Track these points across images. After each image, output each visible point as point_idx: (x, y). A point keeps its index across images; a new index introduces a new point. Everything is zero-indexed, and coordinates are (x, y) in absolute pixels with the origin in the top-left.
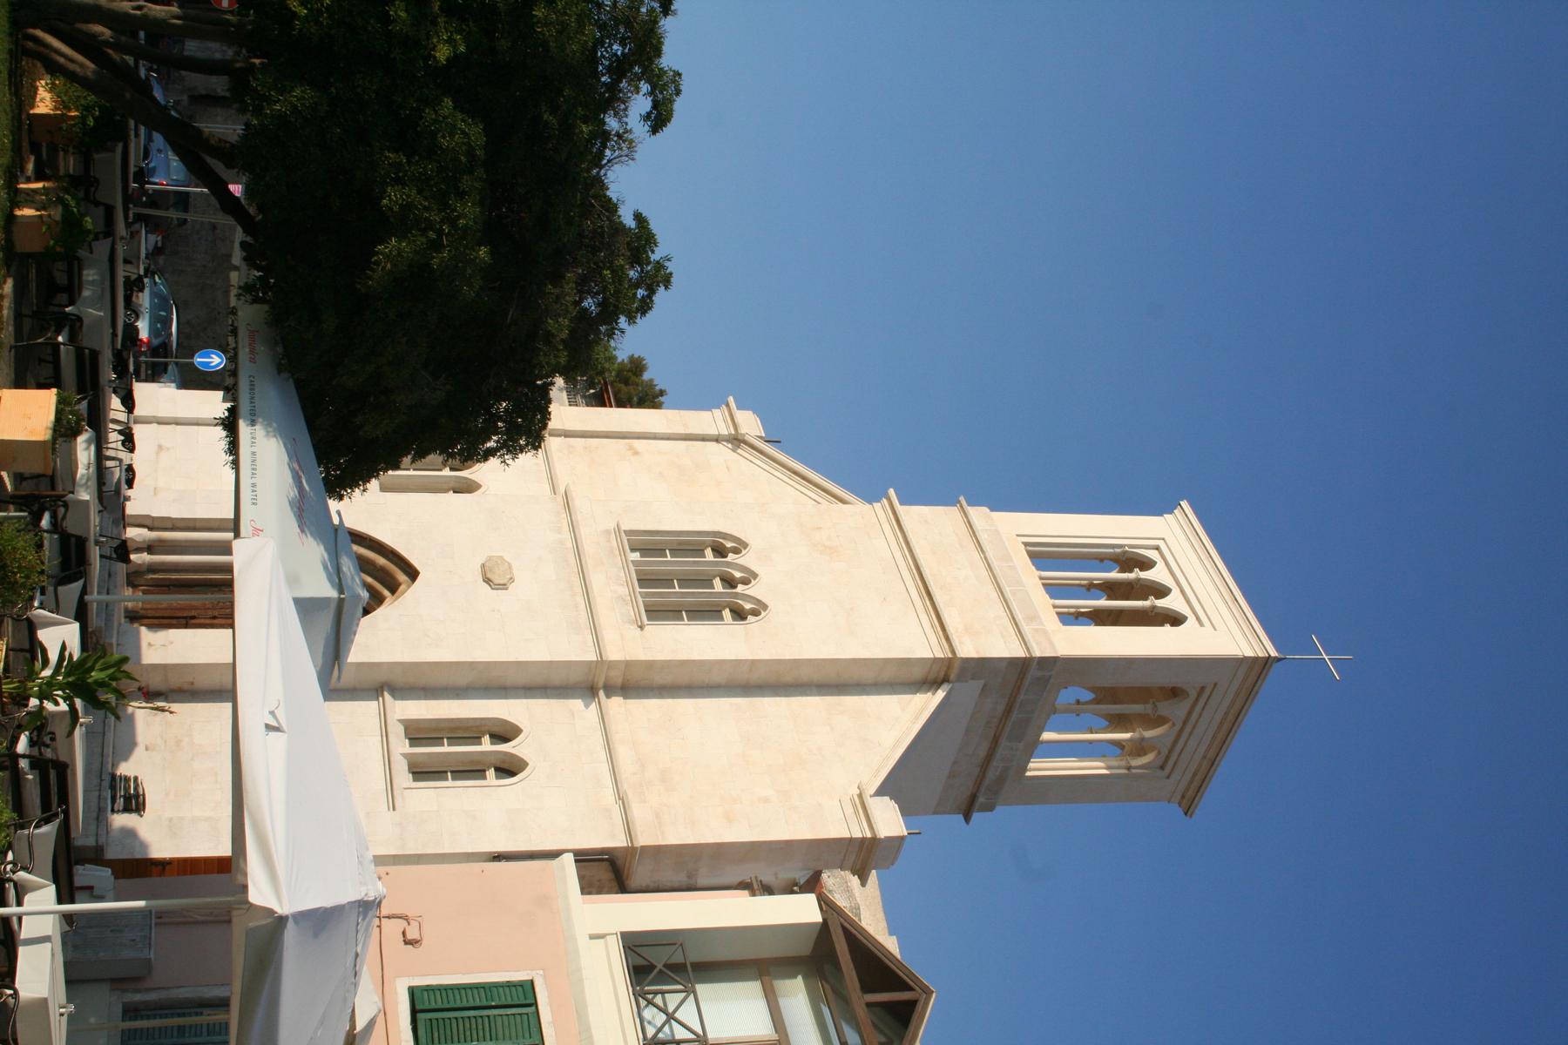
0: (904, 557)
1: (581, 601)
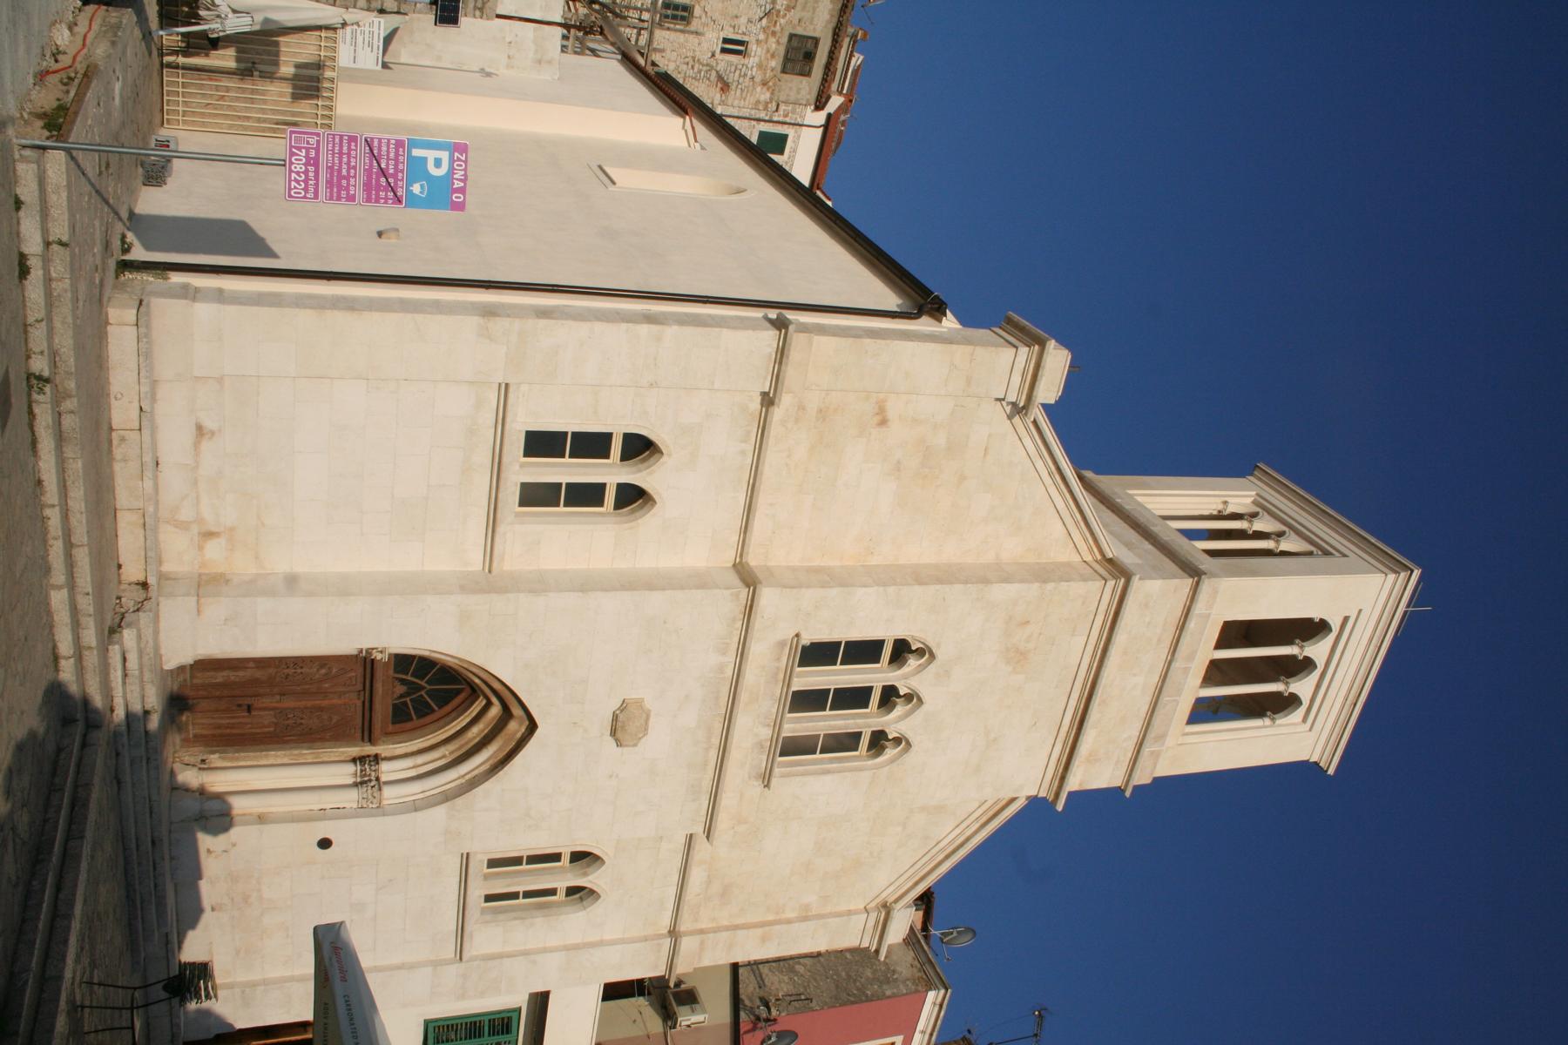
0: (1090, 667)
1: (713, 755)
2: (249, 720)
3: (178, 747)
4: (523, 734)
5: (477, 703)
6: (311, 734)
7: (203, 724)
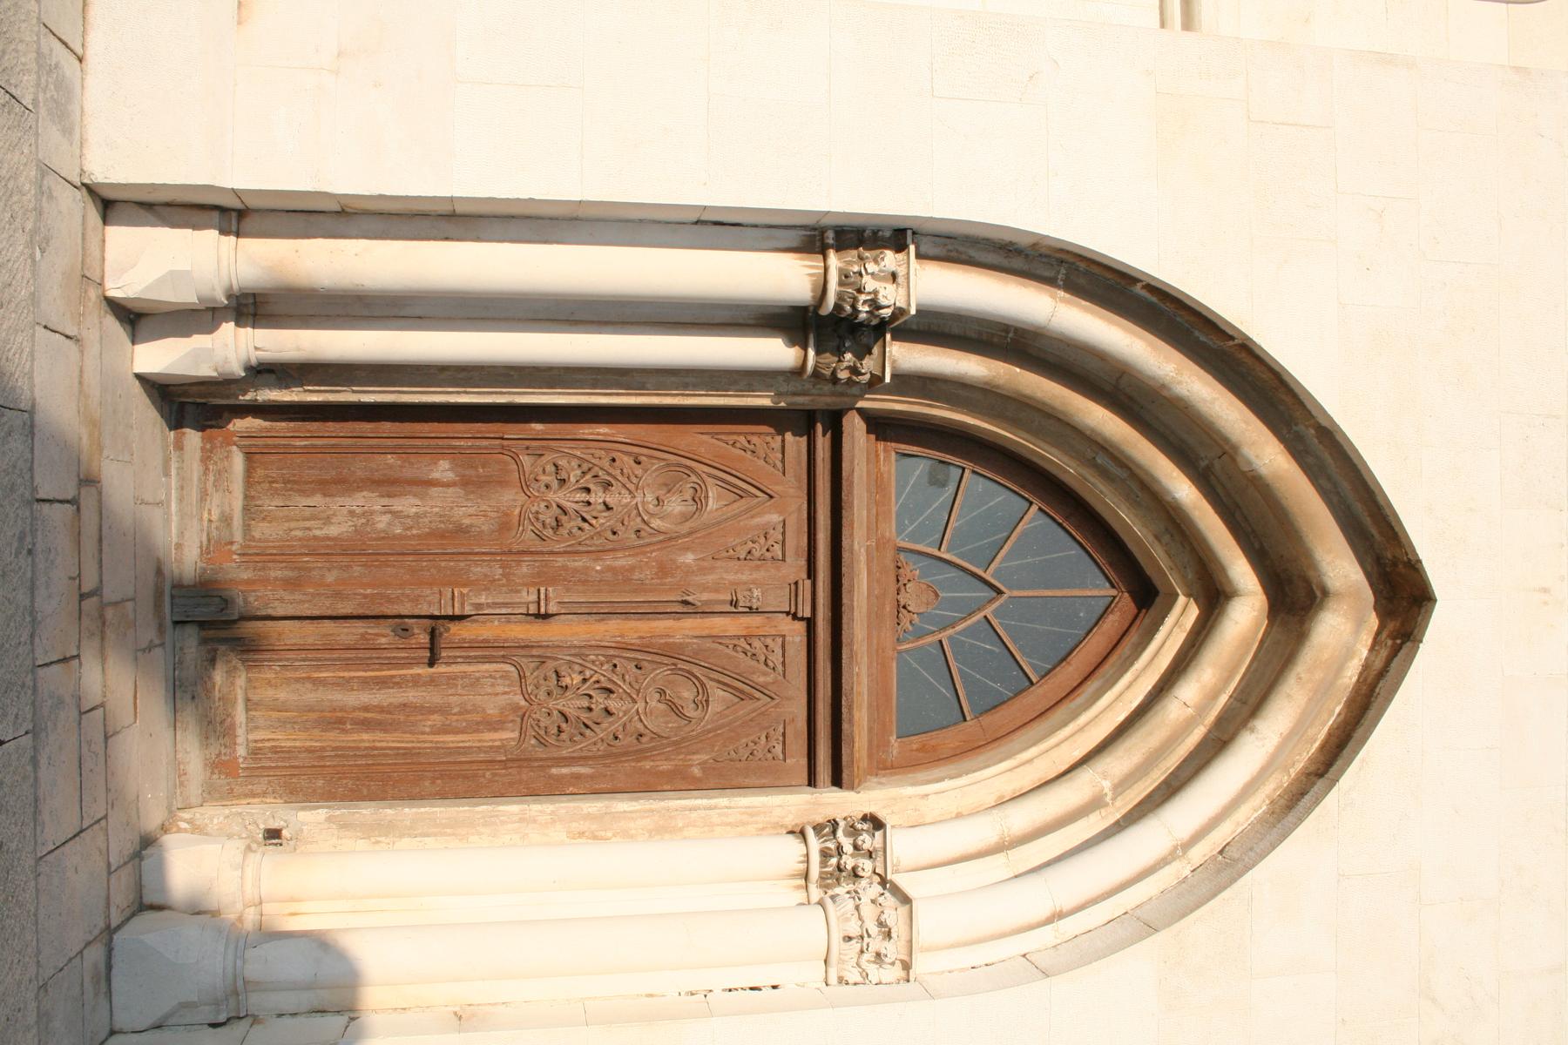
2: (431, 697)
3: (194, 789)
4: (1366, 666)
5: (1169, 621)
6: (641, 755)
7: (281, 708)
